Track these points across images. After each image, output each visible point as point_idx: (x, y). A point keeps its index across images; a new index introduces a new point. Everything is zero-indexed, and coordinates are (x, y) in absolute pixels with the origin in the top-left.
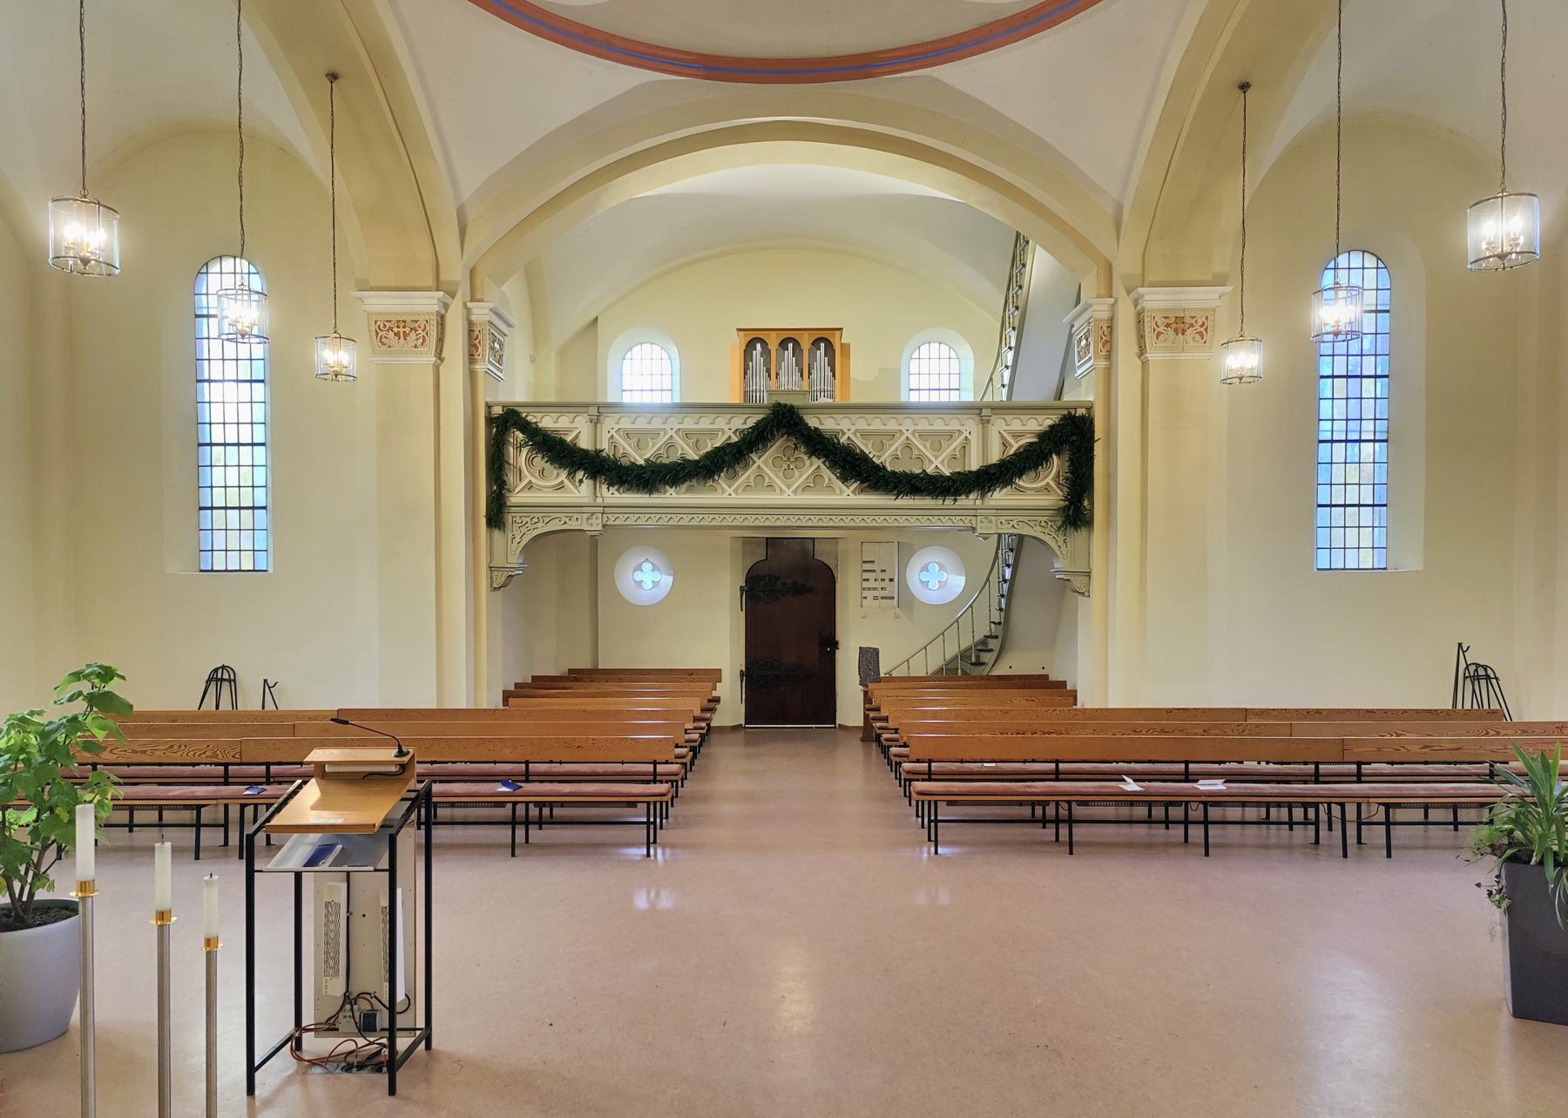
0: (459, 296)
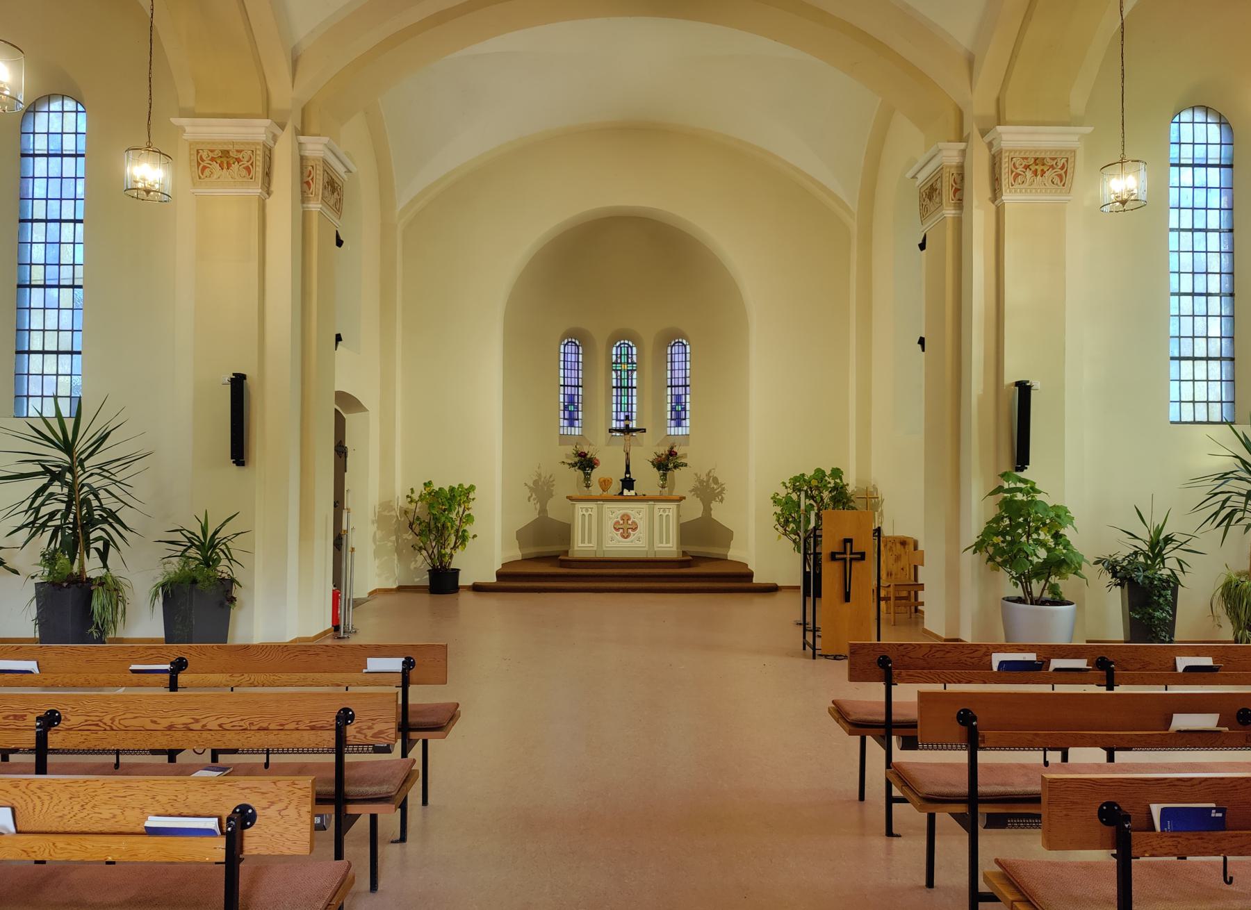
0: (289, 128)
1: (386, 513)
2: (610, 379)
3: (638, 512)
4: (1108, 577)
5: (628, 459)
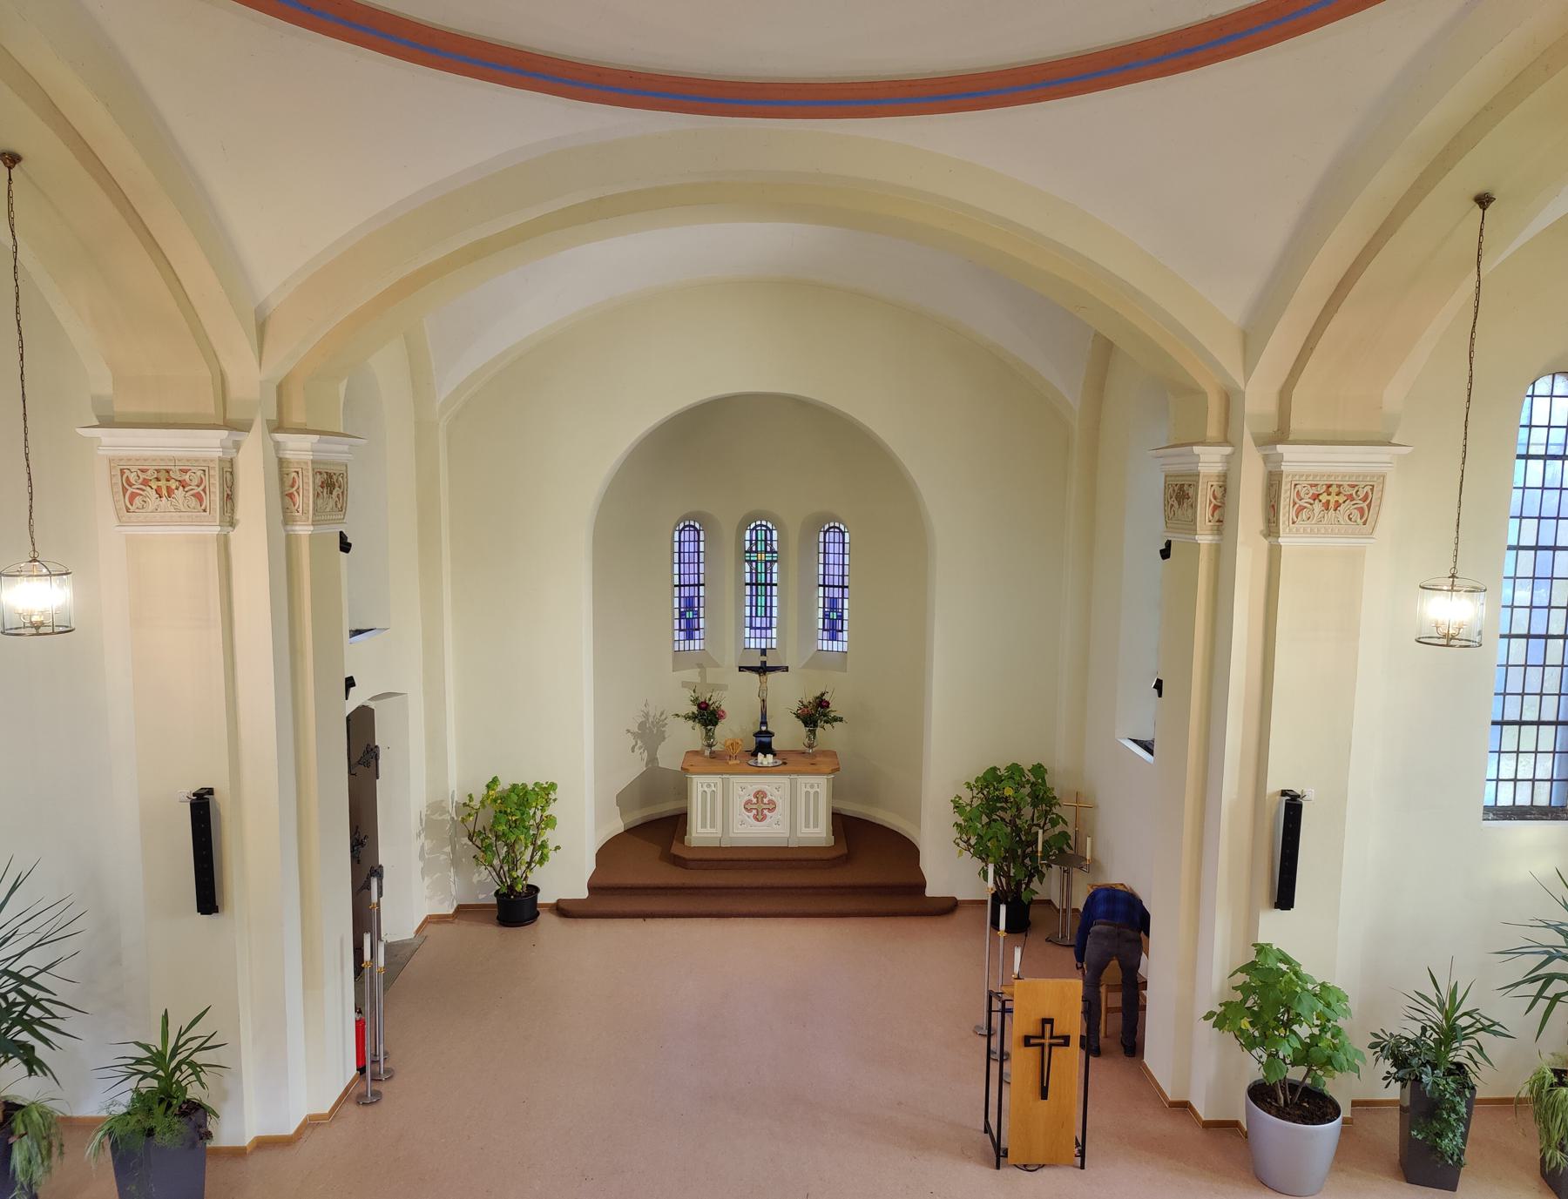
1: (436, 817)
2: (742, 572)
3: (776, 786)
4: (1387, 1066)
5: (764, 708)
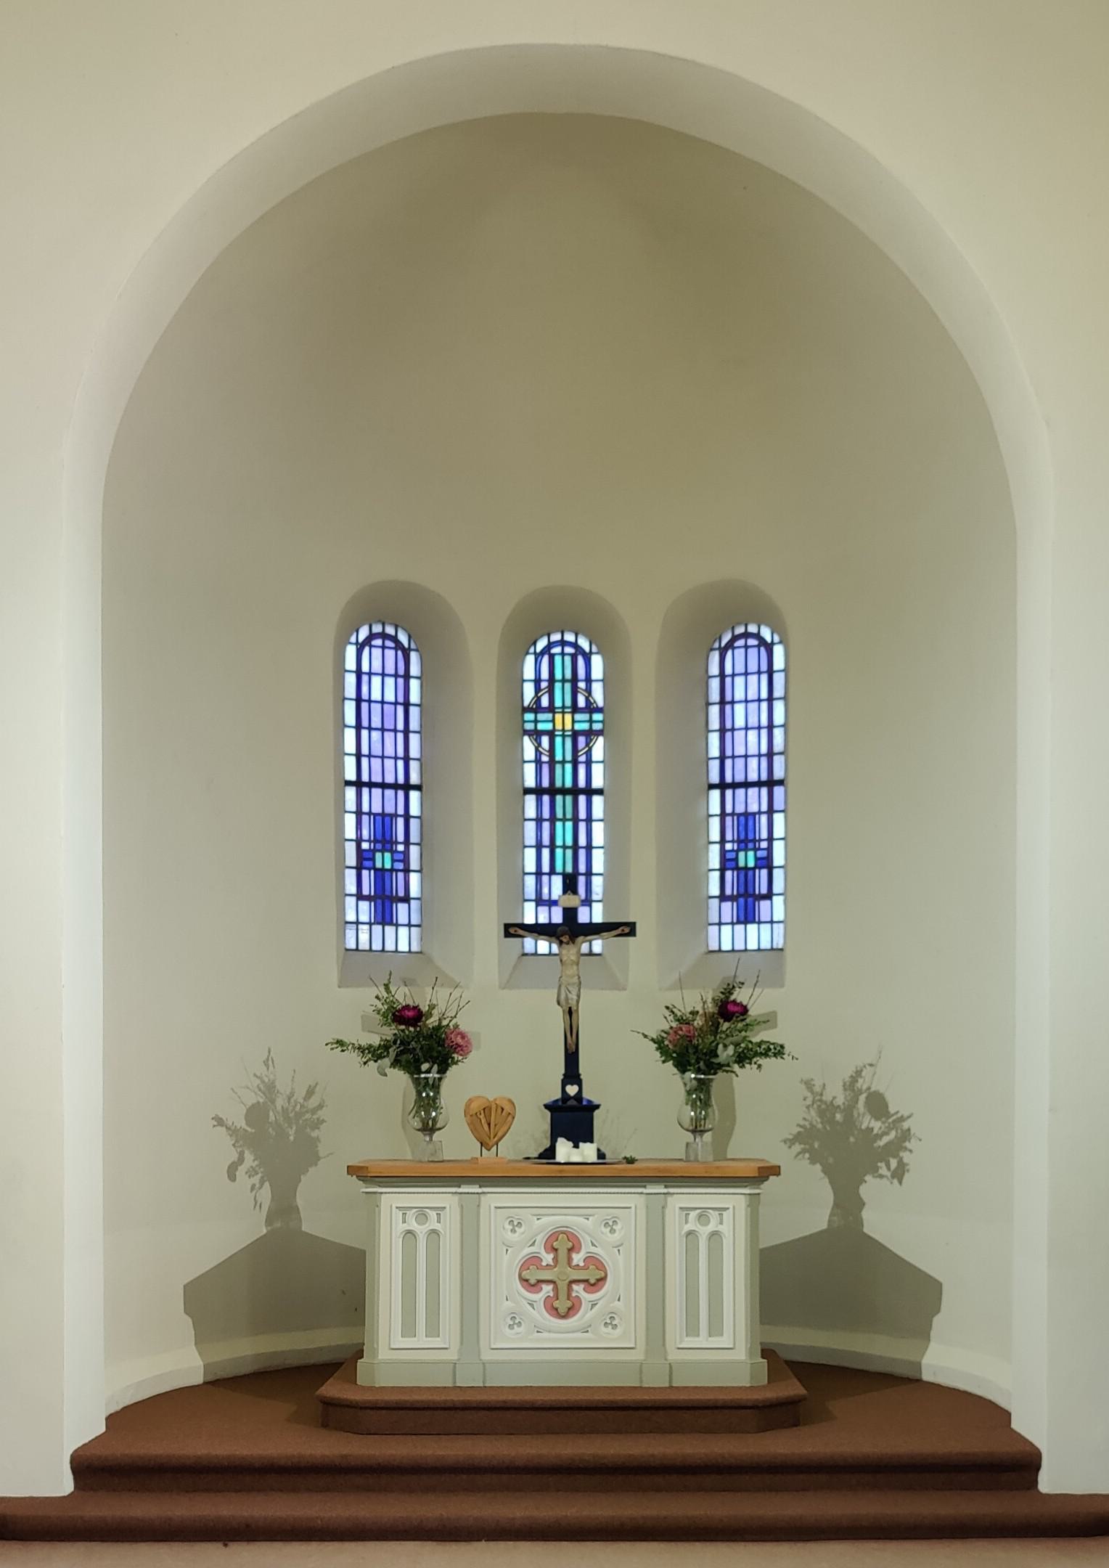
3: (607, 1222)
5: (572, 1033)
